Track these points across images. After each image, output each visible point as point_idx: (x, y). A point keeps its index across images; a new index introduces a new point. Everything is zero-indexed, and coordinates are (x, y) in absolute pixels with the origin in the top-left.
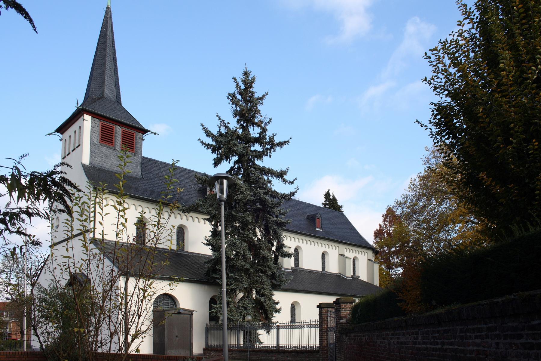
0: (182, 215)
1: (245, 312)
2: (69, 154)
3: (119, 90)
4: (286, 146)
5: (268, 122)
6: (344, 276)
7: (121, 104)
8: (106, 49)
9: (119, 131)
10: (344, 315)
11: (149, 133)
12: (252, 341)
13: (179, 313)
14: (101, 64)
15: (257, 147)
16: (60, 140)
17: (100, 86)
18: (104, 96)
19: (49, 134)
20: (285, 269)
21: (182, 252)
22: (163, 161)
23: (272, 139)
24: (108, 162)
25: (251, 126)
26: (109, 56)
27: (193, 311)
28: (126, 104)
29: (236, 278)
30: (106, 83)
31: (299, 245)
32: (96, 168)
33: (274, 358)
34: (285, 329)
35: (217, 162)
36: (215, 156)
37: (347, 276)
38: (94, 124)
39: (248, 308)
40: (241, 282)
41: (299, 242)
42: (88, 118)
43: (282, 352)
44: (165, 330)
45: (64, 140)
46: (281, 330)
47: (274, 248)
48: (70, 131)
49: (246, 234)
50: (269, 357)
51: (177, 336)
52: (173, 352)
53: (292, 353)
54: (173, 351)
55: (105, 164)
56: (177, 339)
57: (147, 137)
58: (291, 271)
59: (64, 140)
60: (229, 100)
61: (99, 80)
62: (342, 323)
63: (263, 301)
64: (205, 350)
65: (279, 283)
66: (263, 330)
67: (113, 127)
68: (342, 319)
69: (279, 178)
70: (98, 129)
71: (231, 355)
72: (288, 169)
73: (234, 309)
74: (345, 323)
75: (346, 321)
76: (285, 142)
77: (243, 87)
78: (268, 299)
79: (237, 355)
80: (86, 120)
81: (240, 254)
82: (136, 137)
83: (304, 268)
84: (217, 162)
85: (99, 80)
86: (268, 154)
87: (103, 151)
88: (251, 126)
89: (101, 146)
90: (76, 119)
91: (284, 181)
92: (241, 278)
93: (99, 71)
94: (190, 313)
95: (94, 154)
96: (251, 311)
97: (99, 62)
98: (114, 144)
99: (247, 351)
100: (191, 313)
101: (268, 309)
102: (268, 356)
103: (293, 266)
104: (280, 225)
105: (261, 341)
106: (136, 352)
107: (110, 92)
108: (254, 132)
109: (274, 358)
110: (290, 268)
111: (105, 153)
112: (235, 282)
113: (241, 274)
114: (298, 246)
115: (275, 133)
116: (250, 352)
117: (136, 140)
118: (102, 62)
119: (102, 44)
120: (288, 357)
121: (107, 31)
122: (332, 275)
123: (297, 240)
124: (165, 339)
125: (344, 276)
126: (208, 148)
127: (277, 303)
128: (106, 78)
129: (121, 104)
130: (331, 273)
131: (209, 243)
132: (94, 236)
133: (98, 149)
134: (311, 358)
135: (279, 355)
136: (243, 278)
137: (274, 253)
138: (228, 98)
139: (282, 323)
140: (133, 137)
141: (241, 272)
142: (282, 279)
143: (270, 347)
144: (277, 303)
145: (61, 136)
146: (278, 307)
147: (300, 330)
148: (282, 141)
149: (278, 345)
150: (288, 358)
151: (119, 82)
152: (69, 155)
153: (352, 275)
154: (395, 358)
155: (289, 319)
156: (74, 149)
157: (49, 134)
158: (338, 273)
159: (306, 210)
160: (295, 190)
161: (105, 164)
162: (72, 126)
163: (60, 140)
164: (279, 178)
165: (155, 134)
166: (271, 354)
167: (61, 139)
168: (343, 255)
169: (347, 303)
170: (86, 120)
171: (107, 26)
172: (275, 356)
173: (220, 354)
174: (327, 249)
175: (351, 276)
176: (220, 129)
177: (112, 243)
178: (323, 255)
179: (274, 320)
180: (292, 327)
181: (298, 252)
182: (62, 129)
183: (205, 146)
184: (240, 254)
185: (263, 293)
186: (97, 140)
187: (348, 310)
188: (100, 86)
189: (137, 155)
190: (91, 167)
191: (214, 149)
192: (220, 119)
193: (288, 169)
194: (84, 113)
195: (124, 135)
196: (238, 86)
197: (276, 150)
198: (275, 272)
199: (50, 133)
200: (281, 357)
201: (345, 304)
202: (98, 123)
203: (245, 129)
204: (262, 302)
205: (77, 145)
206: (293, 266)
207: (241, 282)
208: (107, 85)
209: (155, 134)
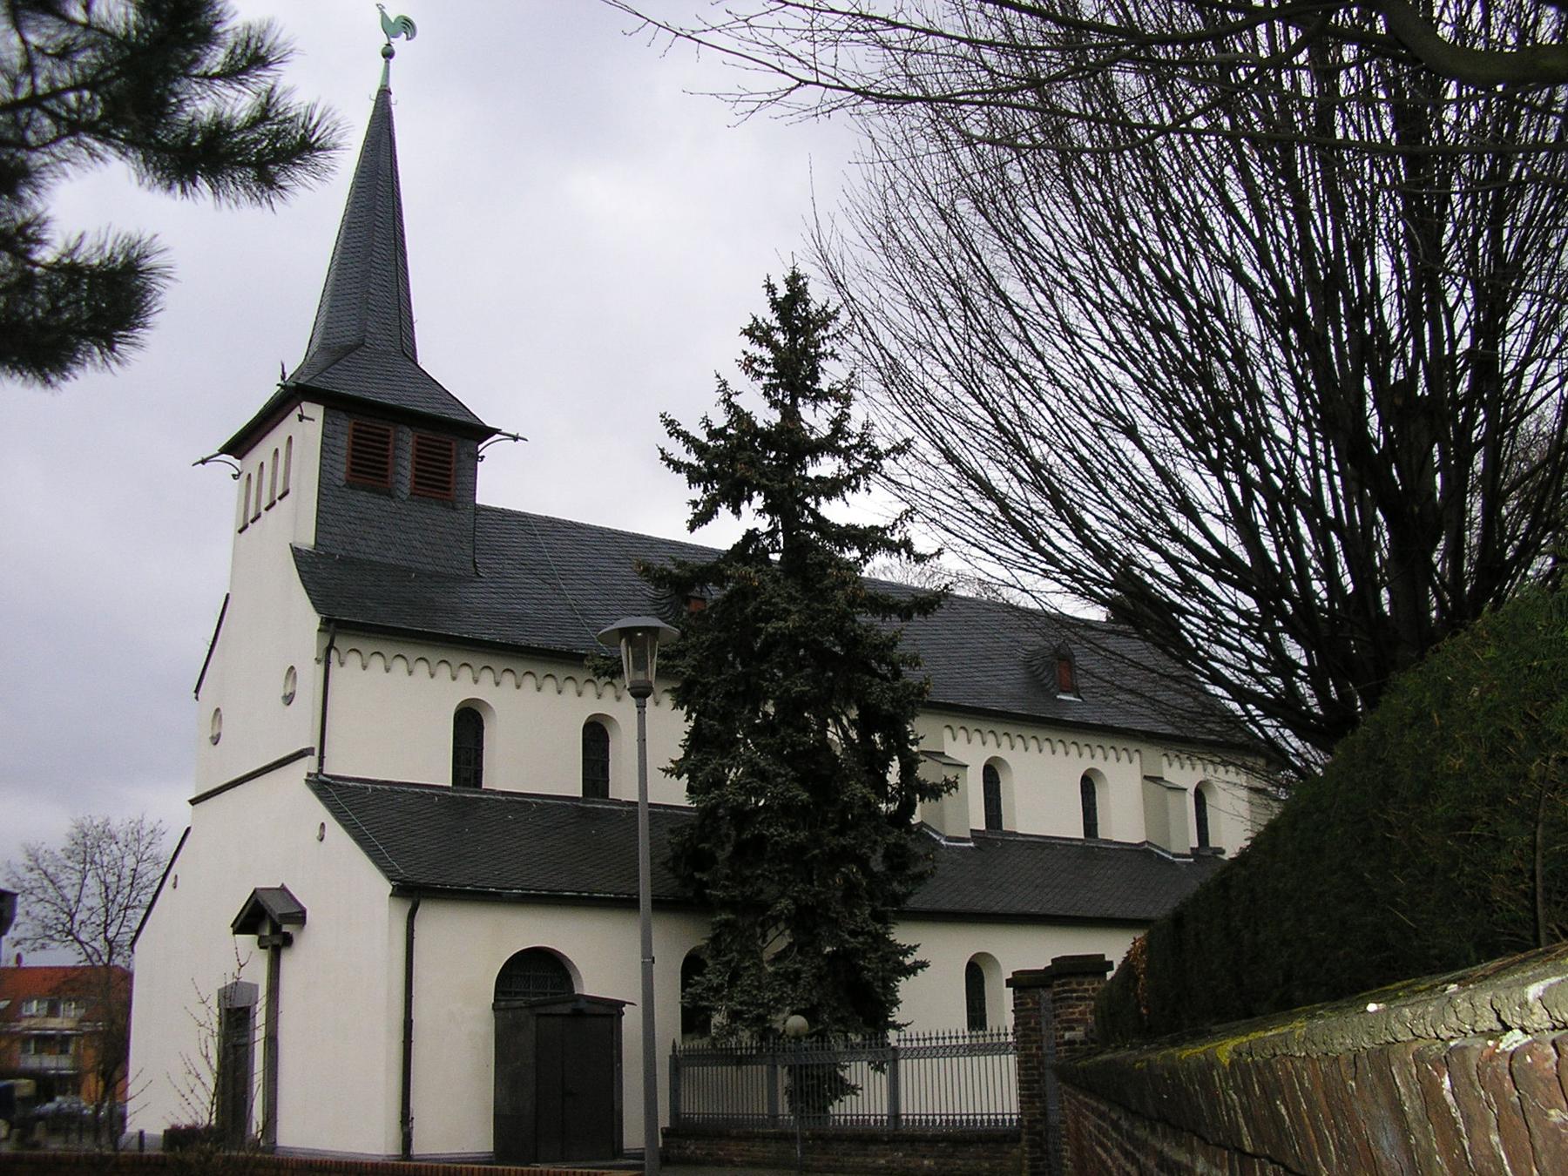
2: (258, 517)
3: (411, 318)
6: (1163, 850)
9: (406, 443)
10: (1077, 1016)
11: (497, 436)
13: (578, 1014)
15: (826, 467)
16: (234, 476)
19: (204, 462)
20: (949, 839)
21: (598, 803)
22: (544, 514)
23: (864, 442)
27: (623, 1004)
28: (431, 358)
33: (882, 1161)
35: (701, 518)
36: (697, 493)
37: (1174, 850)
38: (331, 427)
41: (999, 745)
42: (315, 411)
45: (244, 477)
46: (903, 1062)
48: (262, 452)
53: (938, 1142)
57: (490, 451)
58: (972, 844)
59: (244, 477)
62: (1071, 1042)
68: (1073, 1029)
70: (344, 442)
74: (1082, 1043)
75: (1086, 1034)
84: (701, 518)
90: (279, 416)
94: (613, 1009)
99: (794, 1137)
102: (1533, 878)
104: (920, 701)
106: (883, 1071)
108: (816, 419)
109: (882, 1161)
114: (995, 759)
116: (804, 1139)
117: (459, 461)
120: (924, 1157)
122: (1122, 850)
125: (1163, 850)
126: (679, 471)
129: (415, 357)
130: (1119, 843)
131: (679, 777)
132: (321, 771)
135: (897, 1150)
139: (950, 1038)
145: (237, 462)
149: (895, 1115)
150: (926, 1162)
151: (409, 296)
152: (258, 522)
153: (1196, 845)
155: (958, 1019)
156: (272, 504)
157: (204, 462)
158: (1143, 843)
162: (266, 439)
163: (234, 476)
165: (516, 438)
168: (1156, 780)
169: (1086, 974)
172: (884, 1156)
174: (1098, 763)
175: (1189, 852)
177: (374, 790)
178: (1088, 785)
180: (971, 1050)
182: (239, 446)
183: (668, 465)
186: (341, 471)
187: (1092, 999)
189: (459, 506)
190: (318, 555)
191: (694, 476)
195: (421, 457)
199: (205, 457)
200: (904, 1156)
201: (1080, 979)
202: (345, 424)
203: (791, 414)
205: (279, 493)
209: (516, 438)
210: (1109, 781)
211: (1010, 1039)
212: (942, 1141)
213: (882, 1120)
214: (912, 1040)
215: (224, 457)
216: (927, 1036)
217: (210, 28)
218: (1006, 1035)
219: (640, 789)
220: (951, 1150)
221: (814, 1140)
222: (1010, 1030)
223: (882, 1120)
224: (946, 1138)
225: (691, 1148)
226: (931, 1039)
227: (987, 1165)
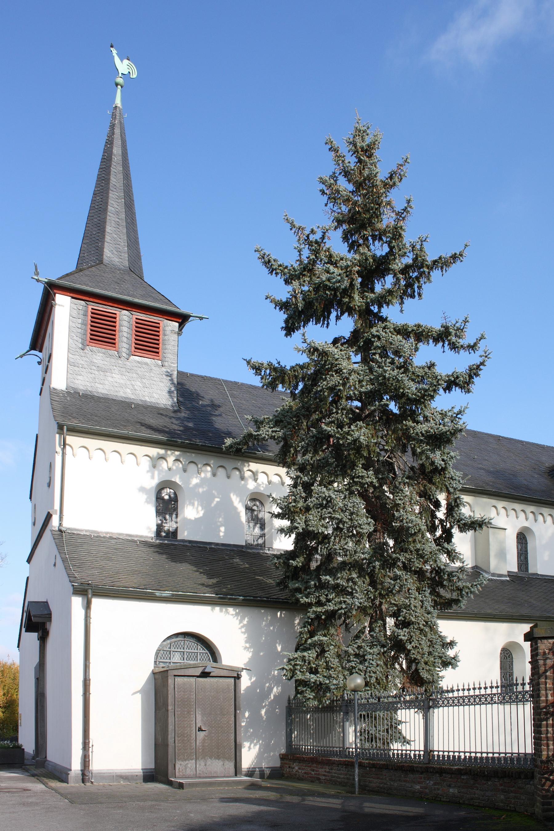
0: (239, 468)
1: (361, 667)
4: (455, 267)
5: (405, 209)
7: (141, 278)
8: (109, 179)
11: (191, 318)
12: (380, 739)
14: (101, 206)
17: (97, 245)
18: (102, 261)
24: (106, 382)
25: (376, 242)
26: (114, 190)
29: (338, 585)
30: (108, 238)
31: (526, 524)
32: (79, 393)
33: (418, 787)
34: (478, 707)
39: (368, 657)
40: (351, 594)
43: (437, 772)
44: (170, 714)
47: (441, 514)
49: (358, 477)
50: (407, 785)
51: (200, 729)
52: (189, 765)
53: (462, 774)
54: (191, 764)
55: (99, 386)
56: (201, 735)
58: (508, 579)
60: (325, 198)
61: (95, 236)
63: (403, 638)
64: (283, 757)
65: (455, 596)
66: (412, 710)
67: (115, 314)
69: (444, 342)
71: (329, 772)
72: (466, 321)
73: (335, 662)
76: (454, 257)
77: (351, 161)
78: (418, 632)
79: (341, 774)
80: (59, 305)
81: (344, 526)
82: (164, 330)
83: (539, 573)
85: (95, 236)
86: (416, 294)
87: (95, 361)
88: (376, 242)
89: (90, 353)
91: (454, 347)
92: (351, 584)
93: (95, 220)
95: (76, 368)
96: (378, 665)
97: (97, 204)
98: (117, 345)
100: (236, 675)
101: (419, 657)
102: (405, 781)
103: (516, 570)
105: (408, 738)
107: (116, 253)
109: (418, 787)
110: (506, 573)
111: (100, 365)
112: (337, 595)
113: (351, 574)
114: (527, 529)
115: (424, 236)
117: (165, 335)
118: (101, 203)
119: (104, 172)
120: (450, 786)
121: (112, 148)
123: (522, 515)
124: (169, 736)
127: (452, 644)
128: (108, 229)
132: (60, 524)
133: (85, 359)
134: (512, 795)
136: (355, 583)
137: (442, 525)
138: (323, 192)
140: (157, 329)
141: (349, 570)
142: (460, 584)
143: (410, 754)
144: (452, 644)
146: (451, 653)
147: (520, 707)
148: (447, 254)
149: (428, 751)
150: (451, 790)
154: (261, 453)
159: (544, 459)
160: (481, 360)
161: (99, 386)
164: (444, 342)
165: (201, 318)
166: (412, 776)
167: (40, 360)
170: (59, 305)
171: (113, 138)
172: (419, 783)
173: (309, 769)
176: (300, 255)
179: (444, 684)
181: (526, 541)
184: (344, 526)
185: (405, 617)
188: (97, 245)
189: (166, 364)
192: (293, 226)
193: (466, 321)
194: (55, 291)
196: (339, 158)
197: (432, 279)
198: (439, 568)
200: (435, 784)
204: (401, 640)
206: (516, 570)
207: (351, 594)
208: (109, 241)
210: (536, 534)
211: (527, 688)
212: (466, 774)
213: (420, 755)
214: (463, 690)
215: (33, 352)
216: (477, 686)
217: (439, 448)
218: (523, 684)
219: (41, 537)
220: (472, 782)
221: (370, 768)
222: (527, 680)
223: (420, 755)
224: (460, 772)
225: (296, 767)
226: (458, 690)
227: (502, 797)
